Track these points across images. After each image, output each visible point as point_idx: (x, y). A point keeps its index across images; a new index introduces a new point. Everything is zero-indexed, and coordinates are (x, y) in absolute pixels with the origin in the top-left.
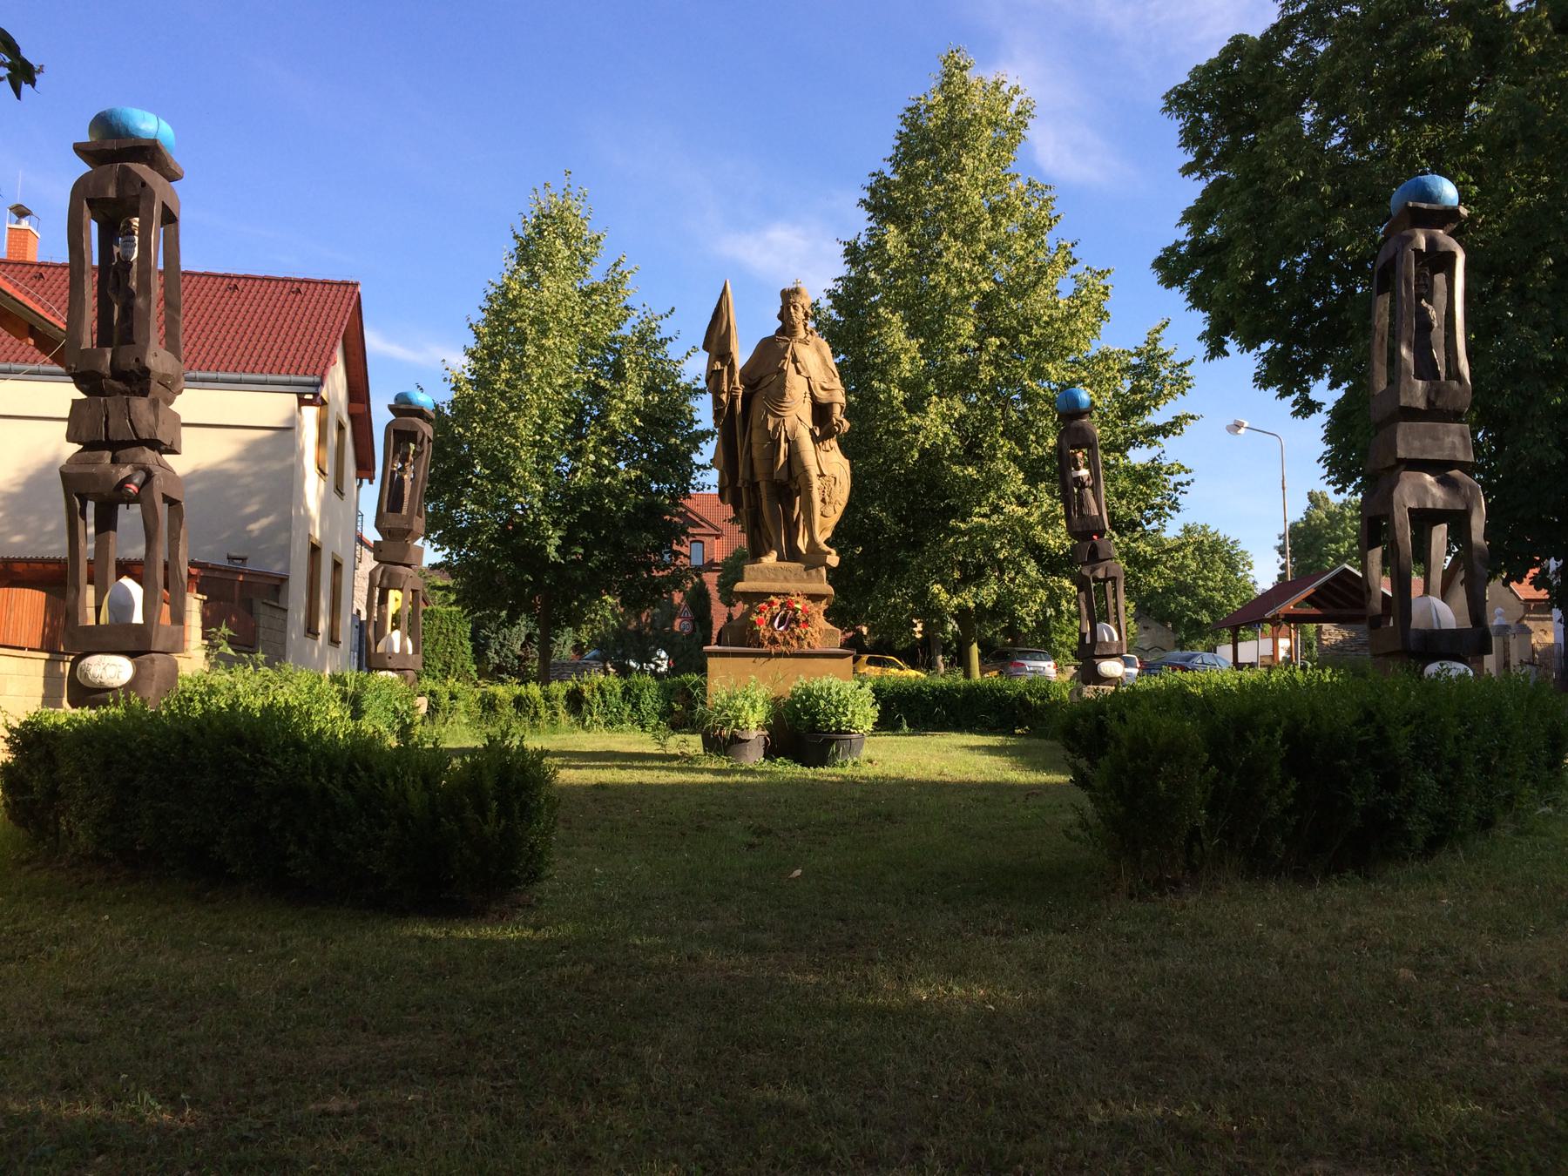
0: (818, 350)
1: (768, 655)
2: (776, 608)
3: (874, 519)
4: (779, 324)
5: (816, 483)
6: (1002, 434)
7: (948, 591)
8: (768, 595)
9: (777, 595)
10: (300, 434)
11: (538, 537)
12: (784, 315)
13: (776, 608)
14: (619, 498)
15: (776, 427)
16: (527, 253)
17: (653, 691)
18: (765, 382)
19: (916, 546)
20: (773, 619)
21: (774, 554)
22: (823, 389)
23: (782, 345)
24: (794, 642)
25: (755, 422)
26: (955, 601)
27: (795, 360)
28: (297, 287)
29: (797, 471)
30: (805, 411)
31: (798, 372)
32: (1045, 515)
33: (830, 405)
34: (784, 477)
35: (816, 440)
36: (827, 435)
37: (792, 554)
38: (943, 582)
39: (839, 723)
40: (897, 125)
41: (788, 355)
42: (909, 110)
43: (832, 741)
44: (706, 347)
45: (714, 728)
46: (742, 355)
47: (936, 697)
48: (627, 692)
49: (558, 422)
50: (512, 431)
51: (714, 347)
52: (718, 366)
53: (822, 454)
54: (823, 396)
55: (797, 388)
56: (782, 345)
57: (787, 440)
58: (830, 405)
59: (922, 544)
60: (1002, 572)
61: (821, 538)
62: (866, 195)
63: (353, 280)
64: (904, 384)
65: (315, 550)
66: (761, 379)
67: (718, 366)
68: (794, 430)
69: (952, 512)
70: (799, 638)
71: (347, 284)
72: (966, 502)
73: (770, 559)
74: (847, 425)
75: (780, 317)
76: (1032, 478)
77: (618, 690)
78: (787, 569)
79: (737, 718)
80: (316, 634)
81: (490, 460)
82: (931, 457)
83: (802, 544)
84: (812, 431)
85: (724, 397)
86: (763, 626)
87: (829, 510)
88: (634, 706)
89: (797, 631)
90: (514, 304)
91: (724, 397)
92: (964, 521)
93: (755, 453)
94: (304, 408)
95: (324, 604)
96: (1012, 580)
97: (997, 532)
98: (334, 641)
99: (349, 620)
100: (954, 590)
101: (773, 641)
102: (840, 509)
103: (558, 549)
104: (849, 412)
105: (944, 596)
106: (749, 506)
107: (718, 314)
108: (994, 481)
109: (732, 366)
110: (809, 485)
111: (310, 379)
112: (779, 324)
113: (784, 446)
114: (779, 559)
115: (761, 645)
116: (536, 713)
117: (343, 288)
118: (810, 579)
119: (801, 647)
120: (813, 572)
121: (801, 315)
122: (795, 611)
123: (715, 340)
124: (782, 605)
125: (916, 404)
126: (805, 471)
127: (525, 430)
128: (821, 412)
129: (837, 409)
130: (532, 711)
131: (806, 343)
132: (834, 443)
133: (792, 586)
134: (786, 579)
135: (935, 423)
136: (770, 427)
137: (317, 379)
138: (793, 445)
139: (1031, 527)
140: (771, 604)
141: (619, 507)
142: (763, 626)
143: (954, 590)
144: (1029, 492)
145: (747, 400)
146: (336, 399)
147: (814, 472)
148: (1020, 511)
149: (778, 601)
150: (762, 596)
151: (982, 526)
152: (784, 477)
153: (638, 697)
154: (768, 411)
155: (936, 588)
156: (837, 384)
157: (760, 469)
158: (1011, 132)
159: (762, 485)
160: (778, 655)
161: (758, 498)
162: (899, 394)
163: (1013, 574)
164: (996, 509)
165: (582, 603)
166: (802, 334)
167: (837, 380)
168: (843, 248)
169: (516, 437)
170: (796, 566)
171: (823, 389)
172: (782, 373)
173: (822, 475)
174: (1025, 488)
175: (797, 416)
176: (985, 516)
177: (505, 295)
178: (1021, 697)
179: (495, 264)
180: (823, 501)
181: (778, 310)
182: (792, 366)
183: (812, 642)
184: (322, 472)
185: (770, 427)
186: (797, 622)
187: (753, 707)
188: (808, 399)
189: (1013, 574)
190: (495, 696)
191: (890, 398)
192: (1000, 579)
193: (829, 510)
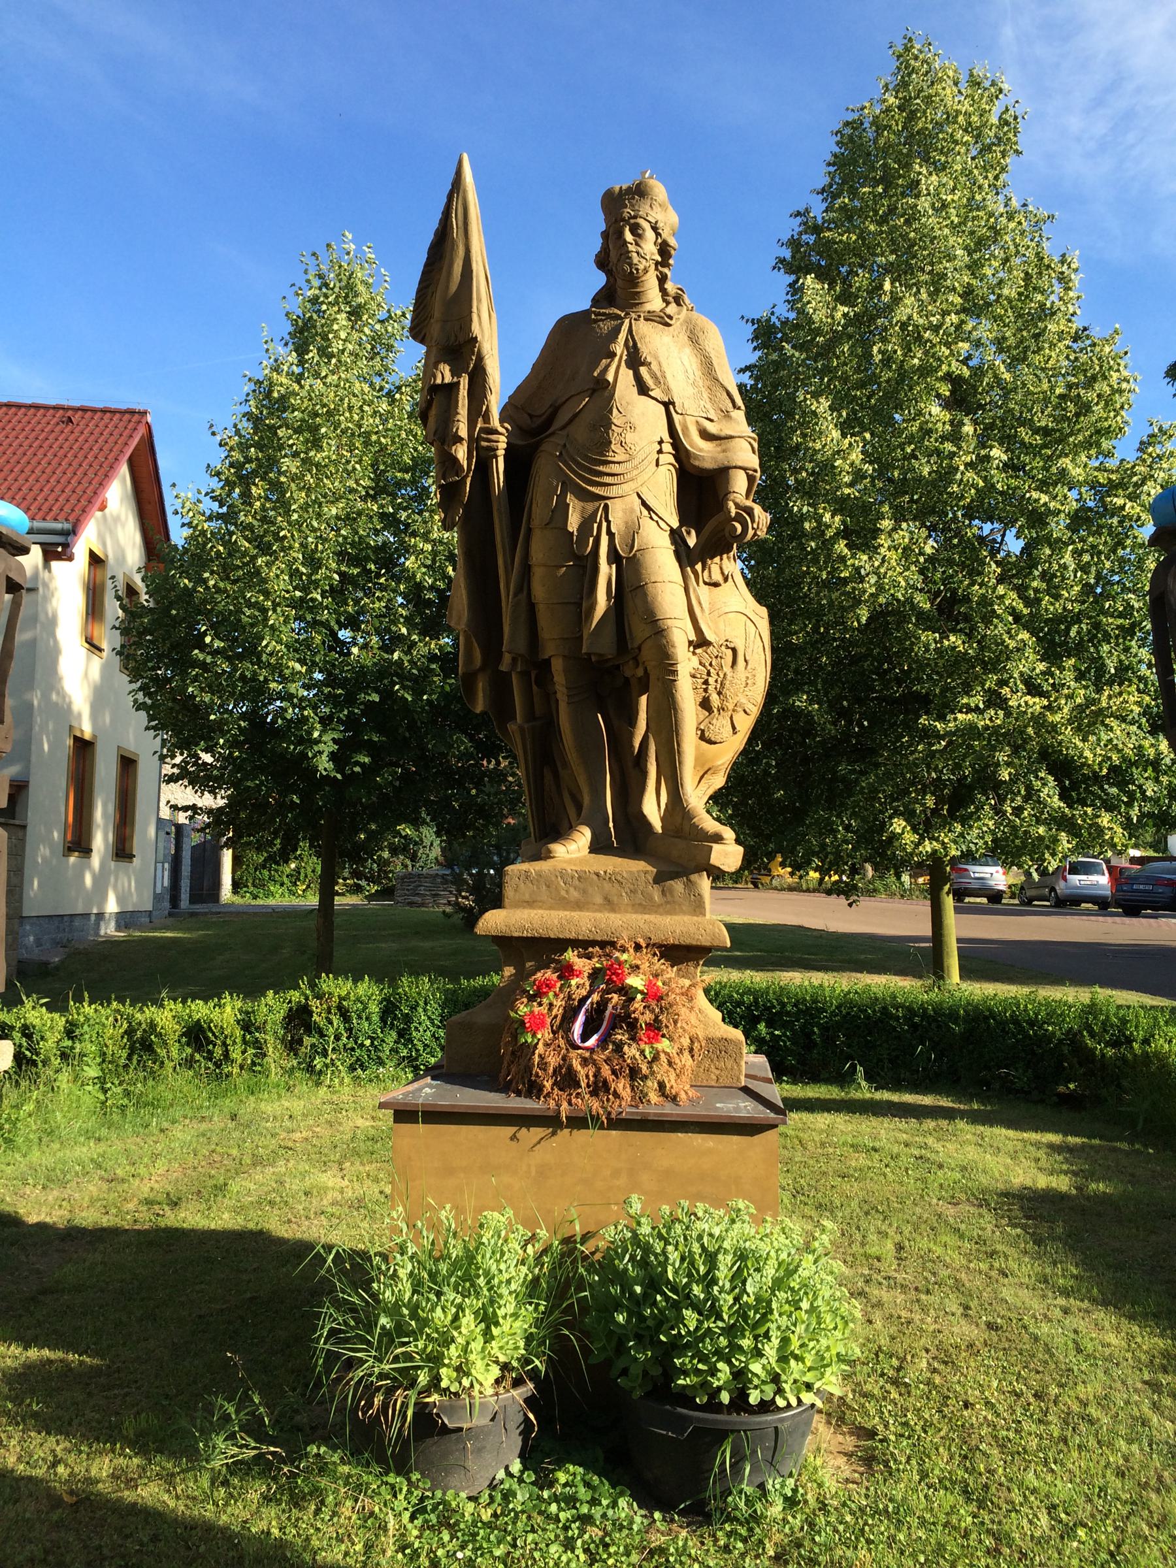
0: (694, 339)
1: (551, 1122)
2: (579, 985)
3: (797, 714)
4: (599, 280)
5: (686, 663)
6: (1000, 580)
7: (915, 830)
8: (563, 944)
9: (583, 945)
10: (47, 599)
11: (300, 741)
12: (613, 259)
13: (579, 985)
14: (419, 683)
15: (586, 524)
16: (305, 335)
17: (434, 1009)
18: (563, 417)
19: (864, 754)
20: (570, 1014)
21: (583, 837)
22: (706, 435)
23: (606, 326)
24: (622, 1086)
25: (538, 513)
26: (928, 847)
27: (635, 360)
28: (67, 415)
29: (639, 632)
30: (660, 486)
31: (643, 389)
32: (1080, 709)
33: (722, 474)
34: (606, 647)
35: (685, 557)
36: (714, 546)
37: (627, 836)
38: (909, 816)
39: (740, 1375)
40: (829, 147)
41: (619, 348)
42: (847, 124)
43: (720, 1435)
44: (418, 331)
45: (370, 1391)
46: (506, 355)
47: (915, 1027)
48: (389, 1010)
49: (331, 571)
50: (255, 578)
51: (435, 329)
52: (445, 374)
53: (703, 591)
54: (704, 453)
55: (638, 425)
56: (606, 326)
57: (614, 557)
58: (722, 474)
59: (874, 752)
60: (1001, 800)
61: (696, 796)
62: (787, 254)
63: (138, 407)
64: (841, 505)
65: (83, 748)
66: (555, 410)
67: (445, 374)
68: (633, 532)
69: (924, 703)
70: (634, 1073)
71: (132, 412)
72: (946, 689)
73: (574, 850)
74: (762, 517)
75: (602, 262)
76: (1052, 652)
77: (374, 1008)
78: (612, 878)
79: (435, 1360)
80: (86, 851)
81: (226, 625)
82: (890, 618)
83: (652, 809)
84: (676, 536)
85: (461, 452)
86: (544, 1035)
87: (720, 726)
88: (401, 1034)
89: (631, 1051)
90: (282, 405)
91: (461, 452)
92: (942, 718)
93: (539, 591)
94: (55, 565)
95: (102, 813)
96: (1018, 811)
97: (996, 737)
98: (122, 851)
99: (152, 831)
100: (925, 827)
101: (567, 1080)
102: (745, 724)
103: (333, 757)
104: (769, 492)
105: (909, 838)
106: (530, 715)
107: (443, 246)
108: (994, 659)
109: (478, 378)
110: (668, 668)
111: (58, 526)
112: (599, 280)
113: (606, 571)
114: (597, 847)
115: (533, 1089)
116: (226, 1054)
117: (127, 416)
118: (669, 905)
119: (640, 1097)
120: (678, 886)
121: (649, 247)
122: (628, 994)
123: (437, 311)
124: (595, 975)
125: (862, 536)
126: (658, 632)
127: (281, 584)
128: (699, 490)
129: (739, 483)
130: (218, 1052)
131: (664, 321)
132: (732, 565)
133: (622, 923)
134: (610, 904)
135: (892, 565)
136: (573, 523)
137: (67, 526)
138: (629, 567)
139: (1053, 729)
140: (567, 972)
141: (418, 694)
142: (544, 1035)
143: (925, 827)
144: (1048, 673)
145: (519, 461)
146: (121, 559)
147: (680, 634)
148: (1037, 704)
149: (583, 965)
150: (544, 950)
151: (971, 727)
152: (606, 647)
153: (408, 1019)
154: (568, 486)
155: (898, 824)
156: (739, 424)
157: (550, 629)
158: (996, 143)
159: (557, 665)
160: (578, 1122)
161: (549, 697)
162: (833, 521)
163: (1019, 801)
164: (995, 700)
165: (371, 835)
166: (653, 301)
167: (740, 415)
168: (750, 328)
169: (267, 594)
170: (637, 868)
171: (706, 435)
172: (602, 390)
173: (701, 642)
174: (1041, 667)
175: (641, 494)
176: (977, 710)
177: (269, 394)
178: (1073, 1038)
179: (266, 351)
180: (705, 704)
181: (597, 244)
182: (626, 375)
183: (671, 1081)
184: (93, 646)
185: (573, 523)
186: (633, 1026)
187: (488, 1320)
188: (668, 458)
189: (1019, 801)
190: (152, 1025)
191: (821, 528)
192: (998, 811)
193: (720, 726)
